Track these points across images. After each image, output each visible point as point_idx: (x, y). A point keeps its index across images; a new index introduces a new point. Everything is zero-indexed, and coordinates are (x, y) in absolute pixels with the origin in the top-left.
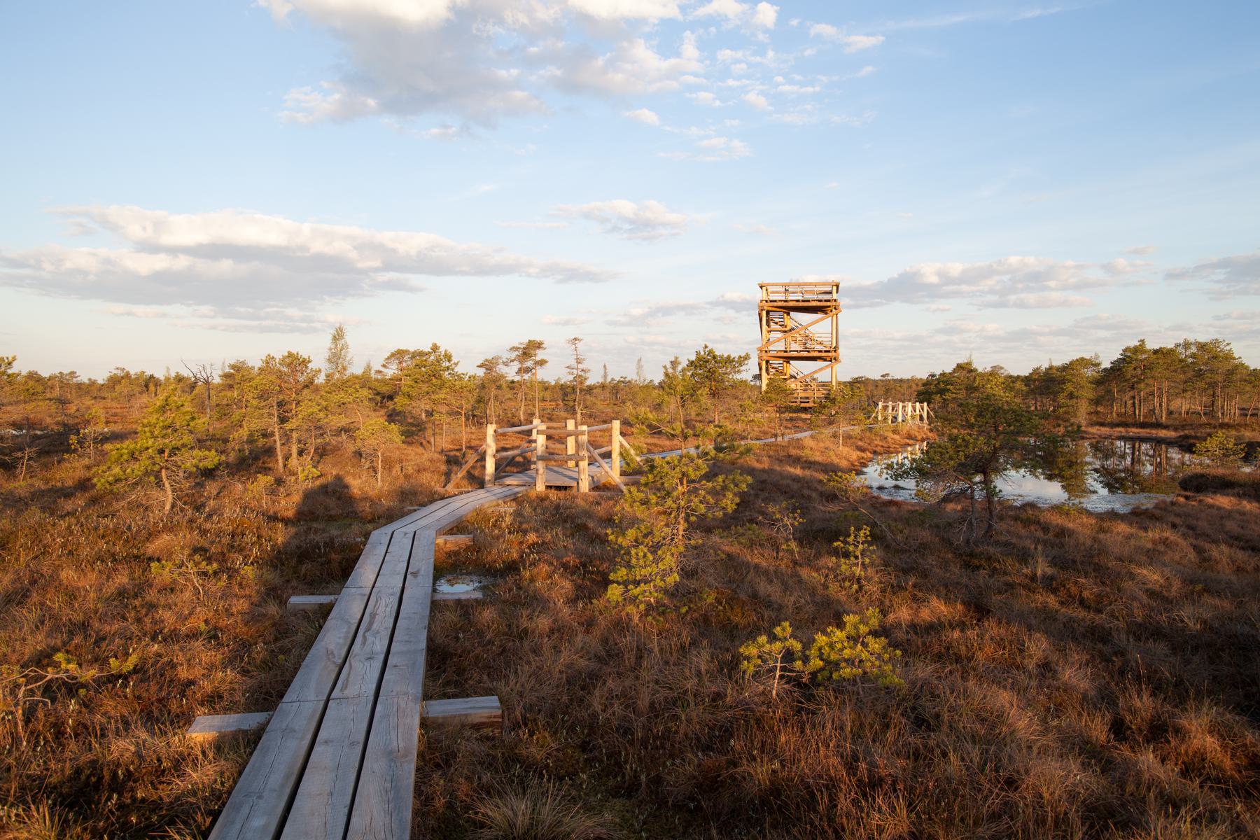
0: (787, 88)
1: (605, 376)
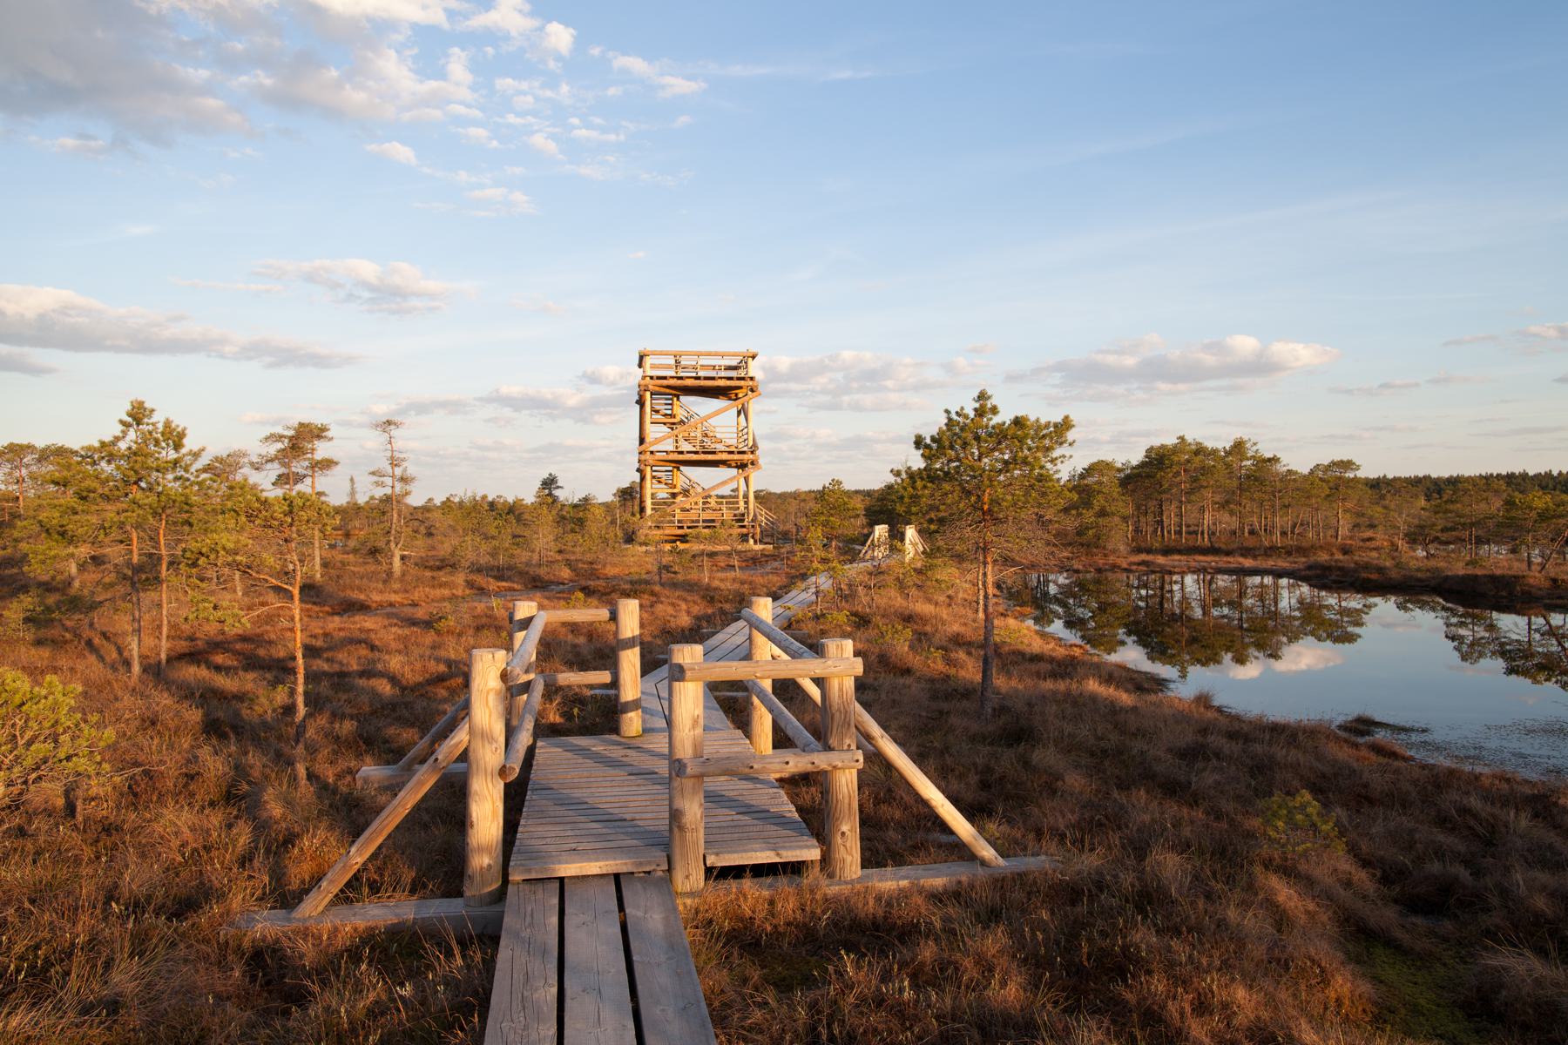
0: (583, 133)
1: (353, 493)
